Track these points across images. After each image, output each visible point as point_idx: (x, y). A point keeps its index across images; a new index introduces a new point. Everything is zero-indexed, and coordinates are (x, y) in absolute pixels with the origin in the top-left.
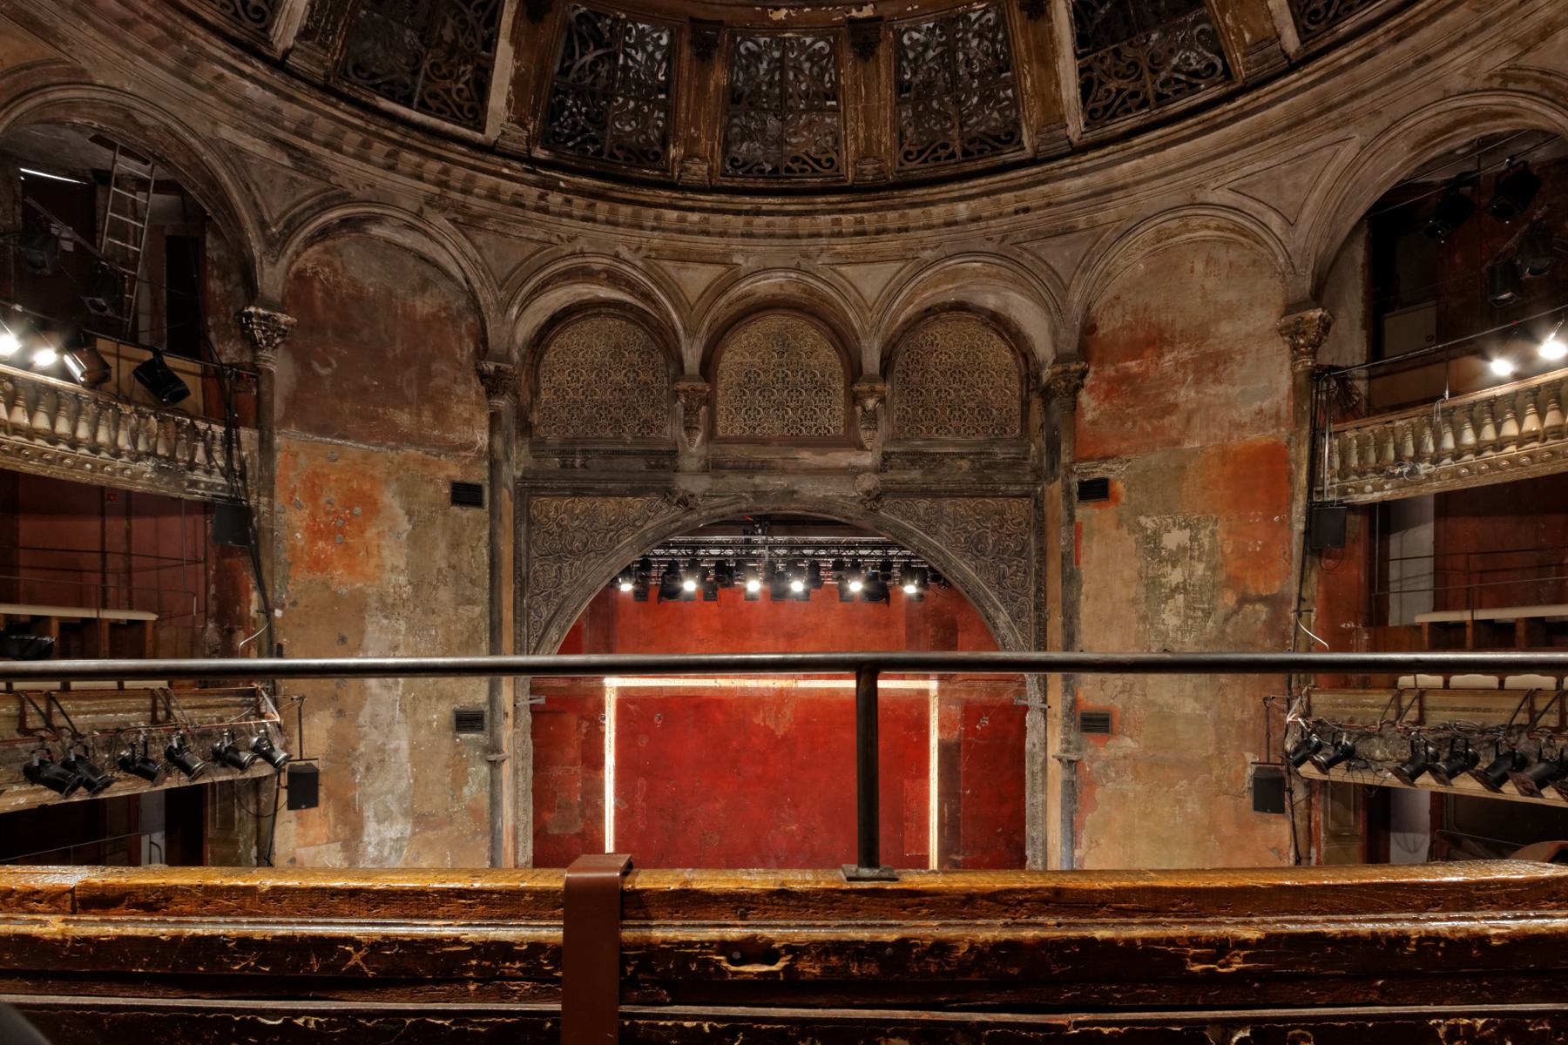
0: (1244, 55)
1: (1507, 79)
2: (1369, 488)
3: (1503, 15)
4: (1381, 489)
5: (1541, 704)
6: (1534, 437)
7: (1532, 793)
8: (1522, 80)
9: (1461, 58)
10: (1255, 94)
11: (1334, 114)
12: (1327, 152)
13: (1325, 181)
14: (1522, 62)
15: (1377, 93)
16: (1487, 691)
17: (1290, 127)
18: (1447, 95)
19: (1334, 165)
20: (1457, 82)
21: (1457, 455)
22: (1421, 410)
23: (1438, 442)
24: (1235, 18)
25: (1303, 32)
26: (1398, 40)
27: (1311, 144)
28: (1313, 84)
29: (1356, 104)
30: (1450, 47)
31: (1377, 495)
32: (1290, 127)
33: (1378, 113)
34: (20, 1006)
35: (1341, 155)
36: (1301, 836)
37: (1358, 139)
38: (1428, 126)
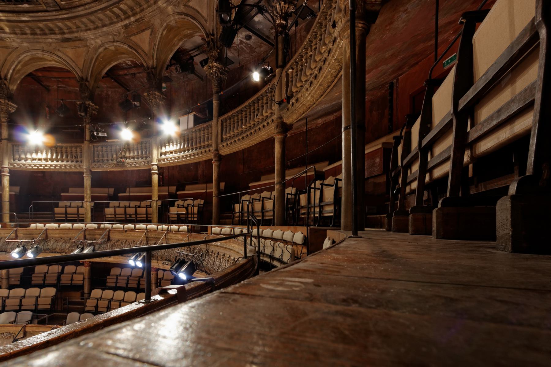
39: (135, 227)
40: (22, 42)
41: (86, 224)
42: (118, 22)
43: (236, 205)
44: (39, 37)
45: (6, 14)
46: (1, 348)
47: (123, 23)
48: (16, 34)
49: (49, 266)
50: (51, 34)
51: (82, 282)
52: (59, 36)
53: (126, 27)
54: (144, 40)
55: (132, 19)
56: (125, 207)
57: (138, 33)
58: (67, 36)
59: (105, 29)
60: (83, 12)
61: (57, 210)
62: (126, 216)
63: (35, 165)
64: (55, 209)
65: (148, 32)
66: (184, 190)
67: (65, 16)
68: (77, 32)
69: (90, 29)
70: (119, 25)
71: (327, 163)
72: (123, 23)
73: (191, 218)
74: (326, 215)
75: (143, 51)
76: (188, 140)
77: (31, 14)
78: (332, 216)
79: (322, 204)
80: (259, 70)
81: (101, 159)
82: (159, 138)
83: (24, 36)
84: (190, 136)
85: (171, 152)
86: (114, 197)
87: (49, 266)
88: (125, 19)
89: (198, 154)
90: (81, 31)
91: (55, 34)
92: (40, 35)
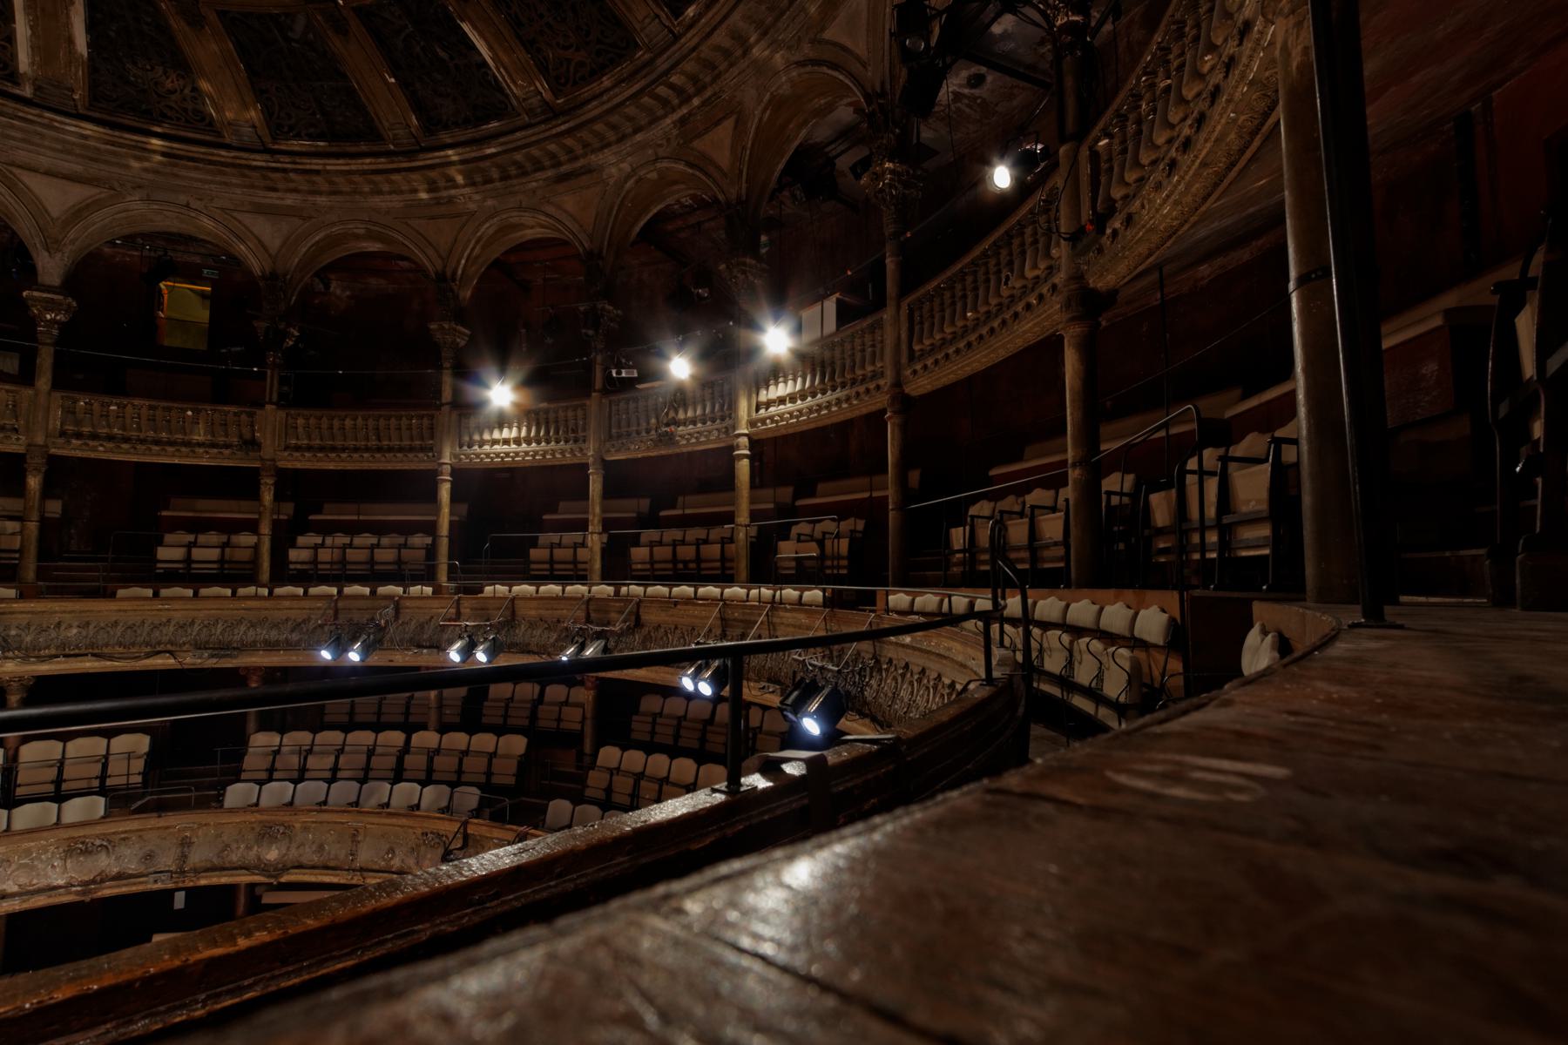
40: (484, 200)
42: (665, 116)
44: (515, 182)
45: (460, 150)
47: (676, 116)
48: (474, 184)
50: (536, 171)
51: (578, 727)
52: (550, 173)
53: (683, 121)
54: (719, 144)
55: (696, 102)
57: (707, 130)
58: (565, 169)
59: (639, 137)
60: (599, 110)
63: (497, 455)
65: (729, 124)
67: (563, 128)
68: (585, 155)
69: (608, 145)
70: (668, 121)
72: (676, 116)
75: (718, 167)
76: (556, 422)
77: (502, 140)
81: (624, 430)
83: (489, 186)
88: (680, 106)
90: (593, 152)
91: (543, 169)
92: (517, 177)
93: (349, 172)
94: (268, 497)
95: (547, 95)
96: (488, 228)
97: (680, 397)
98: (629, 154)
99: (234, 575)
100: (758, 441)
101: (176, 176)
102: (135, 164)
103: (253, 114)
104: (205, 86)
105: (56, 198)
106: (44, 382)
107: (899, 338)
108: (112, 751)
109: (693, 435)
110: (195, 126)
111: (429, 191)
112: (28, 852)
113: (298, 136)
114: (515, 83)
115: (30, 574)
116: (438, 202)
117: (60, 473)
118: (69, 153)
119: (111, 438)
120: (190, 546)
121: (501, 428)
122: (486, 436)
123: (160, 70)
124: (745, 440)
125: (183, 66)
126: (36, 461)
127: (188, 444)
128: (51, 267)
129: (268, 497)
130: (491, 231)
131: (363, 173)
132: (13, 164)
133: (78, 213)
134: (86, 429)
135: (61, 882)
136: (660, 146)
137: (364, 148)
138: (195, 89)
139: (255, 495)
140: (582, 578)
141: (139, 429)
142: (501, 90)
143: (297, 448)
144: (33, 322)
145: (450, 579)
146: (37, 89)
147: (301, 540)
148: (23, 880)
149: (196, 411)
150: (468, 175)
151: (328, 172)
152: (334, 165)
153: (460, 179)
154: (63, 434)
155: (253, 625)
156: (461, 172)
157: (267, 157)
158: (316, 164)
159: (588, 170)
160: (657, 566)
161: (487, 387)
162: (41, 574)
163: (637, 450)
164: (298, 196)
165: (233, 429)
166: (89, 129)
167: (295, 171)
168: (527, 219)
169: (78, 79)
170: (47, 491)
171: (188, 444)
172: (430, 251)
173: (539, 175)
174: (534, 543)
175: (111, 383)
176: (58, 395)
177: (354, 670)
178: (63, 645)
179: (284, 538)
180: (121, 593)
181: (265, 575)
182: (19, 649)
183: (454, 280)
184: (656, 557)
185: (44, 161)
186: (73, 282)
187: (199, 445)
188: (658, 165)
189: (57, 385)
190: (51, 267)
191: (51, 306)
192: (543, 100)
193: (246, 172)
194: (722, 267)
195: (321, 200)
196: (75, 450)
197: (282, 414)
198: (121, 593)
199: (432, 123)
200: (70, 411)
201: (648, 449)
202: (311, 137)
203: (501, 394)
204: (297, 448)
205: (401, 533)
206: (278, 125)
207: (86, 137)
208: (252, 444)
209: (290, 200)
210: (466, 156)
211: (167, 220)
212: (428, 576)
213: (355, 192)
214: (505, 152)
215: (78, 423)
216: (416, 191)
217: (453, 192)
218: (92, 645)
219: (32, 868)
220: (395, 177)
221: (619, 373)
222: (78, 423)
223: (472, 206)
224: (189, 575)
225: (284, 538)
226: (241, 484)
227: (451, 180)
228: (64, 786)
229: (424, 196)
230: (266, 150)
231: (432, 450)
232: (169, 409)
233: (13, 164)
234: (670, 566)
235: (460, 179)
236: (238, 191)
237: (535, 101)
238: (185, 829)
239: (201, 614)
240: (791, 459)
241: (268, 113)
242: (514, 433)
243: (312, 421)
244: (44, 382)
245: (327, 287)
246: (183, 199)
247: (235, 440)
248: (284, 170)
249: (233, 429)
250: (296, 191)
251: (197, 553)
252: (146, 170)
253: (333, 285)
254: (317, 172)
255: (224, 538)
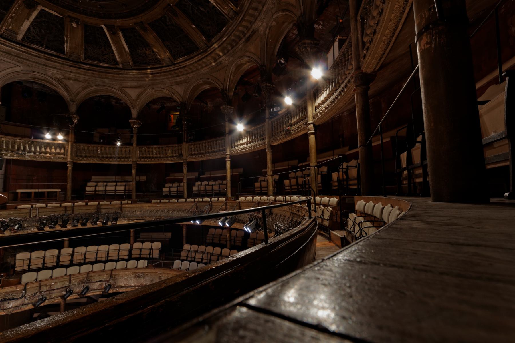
0: (6, 29)
1: (59, 81)
2: (9, 155)
3: (64, 70)
4: (13, 156)
5: (68, 209)
6: (53, 153)
7: (75, 226)
8: (62, 83)
9: (53, 71)
10: (5, 41)
11: (20, 59)
12: (13, 65)
13: (8, 71)
14: (63, 80)
15: (32, 63)
16: (56, 207)
17: (6, 53)
18: (46, 75)
19: (12, 69)
20: (49, 74)
21: (40, 153)
22: (26, 139)
23: (35, 148)
24: (11, 21)
25: (23, 39)
26: (47, 60)
27: (9, 60)
28: (22, 51)
29: (26, 61)
30: (52, 67)
31: (11, 157)
32: (6, 53)
33: (30, 66)
34: (416, 78)
35: (16, 68)
36: (316, 173)
37: (22, 68)
38: (39, 77)
39: (275, 199)
41: (269, 196)
43: (333, 174)
45: (217, 43)
46: (1, 334)
49: (206, 246)
50: (240, 41)
52: (244, 40)
56: (212, 185)
61: (257, 184)
62: (298, 187)
63: (241, 149)
64: (255, 184)
66: (204, 175)
71: (348, 148)
73: (425, 175)
74: (489, 167)
76: (255, 135)
78: (507, 166)
79: (410, 167)
80: (293, 94)
82: (234, 135)
84: (254, 132)
85: (244, 144)
86: (198, 179)
87: (206, 246)
89: (262, 144)
93: (193, 63)
94: (185, 171)
95: (234, 8)
96: (232, 69)
97: (289, 114)
98: (264, 18)
99: (179, 195)
100: (319, 125)
101: (156, 80)
102: (147, 79)
103: (168, 54)
104: (155, 50)
105: (133, 93)
106: (135, 145)
107: (358, 37)
108: (46, 255)
109: (296, 131)
110: (156, 62)
111: (214, 62)
112: (127, 275)
113: (180, 57)
114: (224, 9)
115: (134, 196)
116: (217, 65)
117: (142, 169)
118: (133, 81)
119: (150, 158)
120: (96, 186)
121: (240, 140)
122: (236, 144)
123: (144, 49)
124: (311, 126)
125: (148, 46)
126: (134, 166)
127: (166, 157)
128: (134, 113)
129: (185, 171)
130: (234, 70)
131: (196, 62)
132: (123, 87)
133: (138, 97)
134: (145, 156)
135: (133, 285)
136: (272, 8)
137: (195, 54)
138: (153, 52)
139: (182, 171)
140: (266, 194)
141: (156, 154)
142: (221, 14)
143: (192, 155)
144: (132, 128)
145: (232, 195)
146: (123, 65)
147: (166, 185)
148: (125, 283)
149: (169, 147)
150: (222, 51)
151: (188, 65)
152: (189, 62)
153: (221, 54)
154: (140, 158)
155: (178, 211)
156: (220, 51)
157: (173, 66)
158: (184, 64)
159: (254, 33)
160: (263, 189)
161: (236, 125)
162: (137, 196)
163: (281, 139)
164: (184, 76)
165: (177, 151)
166: (135, 72)
167: (180, 68)
168: (243, 61)
169: (129, 58)
170: (137, 174)
171: (166, 157)
172: (219, 83)
173: (241, 42)
174: (256, 180)
175: (154, 142)
176: (138, 147)
177: (198, 225)
178: (136, 217)
179: (191, 183)
180: (153, 201)
181: (186, 195)
182: (127, 217)
183: (226, 90)
184: (292, 184)
185: (129, 84)
186: (140, 116)
187: (169, 157)
188: (274, 17)
189: (138, 144)
190: (134, 113)
191: (135, 123)
192: (234, 11)
193: (171, 73)
194: (297, 49)
195: (190, 75)
196: (142, 162)
197: (187, 145)
198: (153, 201)
199: (209, 37)
200: (141, 151)
201: (284, 138)
202: (183, 56)
203: (240, 127)
204: (192, 155)
205: (221, 180)
206: (175, 56)
207: (134, 75)
208: (181, 155)
209: (183, 78)
210: (219, 44)
211: (158, 94)
212: (224, 195)
213: (197, 70)
214: (228, 37)
215: (143, 154)
216: (211, 63)
217: (221, 59)
218: (142, 217)
219: (127, 280)
220: (204, 60)
221: (273, 110)
222: (143, 154)
223: (227, 62)
224: (169, 196)
225: (191, 183)
226: (178, 168)
227: (219, 55)
228: (31, 267)
229: (213, 64)
230: (174, 64)
231: (224, 151)
232: (162, 148)
233: (123, 87)
234: (296, 187)
235: (221, 54)
236: (171, 79)
237: (231, 13)
238: (160, 274)
239: (167, 207)
240: (330, 130)
241: (171, 52)
242: (246, 141)
243: (195, 146)
244: (135, 145)
245: (207, 104)
246: (159, 86)
247: (177, 155)
248: (178, 69)
249: (177, 151)
250: (183, 75)
251: (118, 188)
252: (149, 80)
253: (208, 104)
254: (185, 67)
255: (96, 184)
